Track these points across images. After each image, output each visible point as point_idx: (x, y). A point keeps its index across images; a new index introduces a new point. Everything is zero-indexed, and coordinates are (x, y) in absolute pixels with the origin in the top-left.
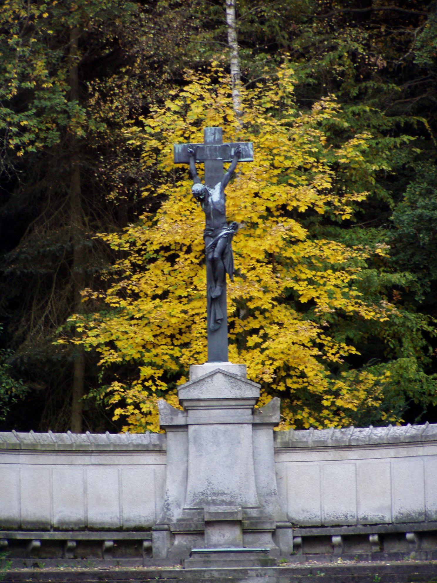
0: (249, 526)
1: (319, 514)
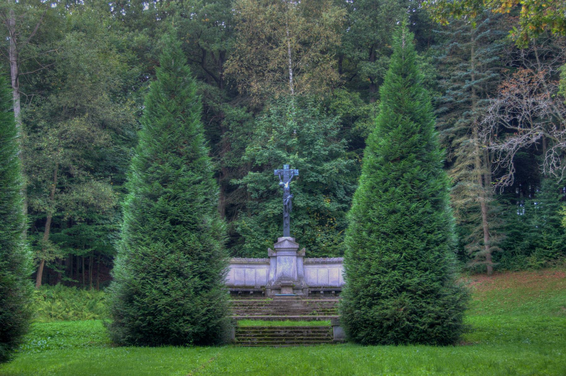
0: (295, 288)
1: (254, 280)
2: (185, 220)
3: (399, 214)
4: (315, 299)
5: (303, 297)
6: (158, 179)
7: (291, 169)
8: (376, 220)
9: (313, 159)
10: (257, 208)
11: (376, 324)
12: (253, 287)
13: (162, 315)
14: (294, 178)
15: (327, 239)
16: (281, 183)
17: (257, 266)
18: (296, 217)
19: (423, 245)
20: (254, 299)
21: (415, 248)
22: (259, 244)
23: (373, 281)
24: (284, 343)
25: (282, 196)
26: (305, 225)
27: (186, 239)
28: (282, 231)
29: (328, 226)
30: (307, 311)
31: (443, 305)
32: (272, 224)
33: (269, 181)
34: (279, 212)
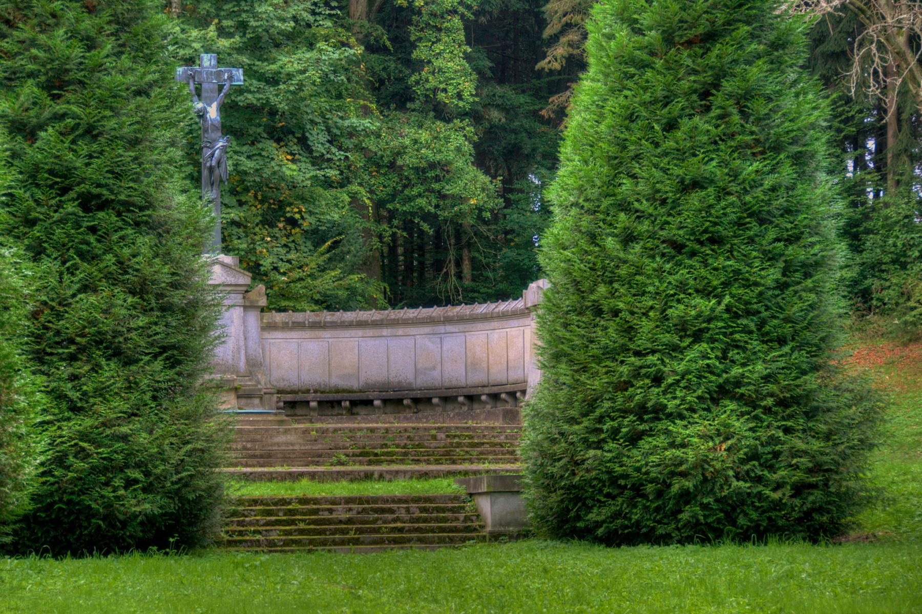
2: (122, 197)
3: (711, 189)
6: (31, 75)
8: (645, 206)
11: (650, 488)
13: (68, 468)
19: (773, 274)
21: (756, 284)
23: (643, 371)
24: (356, 542)
27: (126, 252)
30: (320, 456)
31: (828, 437)
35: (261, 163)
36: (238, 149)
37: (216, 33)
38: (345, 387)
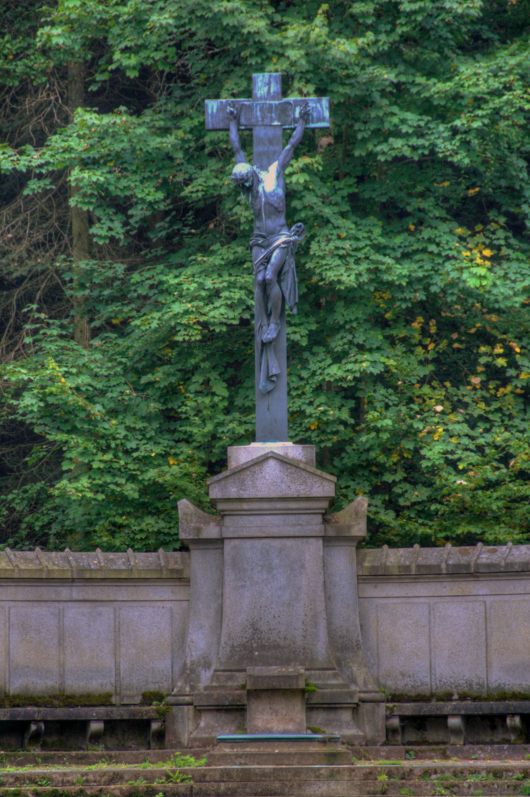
1: (109, 662)
4: (418, 756)
5: (362, 748)
7: (293, 98)
9: (406, 39)
10: (122, 298)
12: (105, 700)
14: (308, 143)
15: (480, 449)
16: (241, 168)
17: (123, 593)
18: (317, 339)
20: (110, 759)
22: (132, 478)
25: (247, 235)
26: (363, 378)
28: (248, 410)
29: (484, 385)
32: (198, 378)
33: (179, 155)
34: (233, 316)
35: (428, 266)
36: (382, 241)
37: (326, 30)
38: (517, 689)
